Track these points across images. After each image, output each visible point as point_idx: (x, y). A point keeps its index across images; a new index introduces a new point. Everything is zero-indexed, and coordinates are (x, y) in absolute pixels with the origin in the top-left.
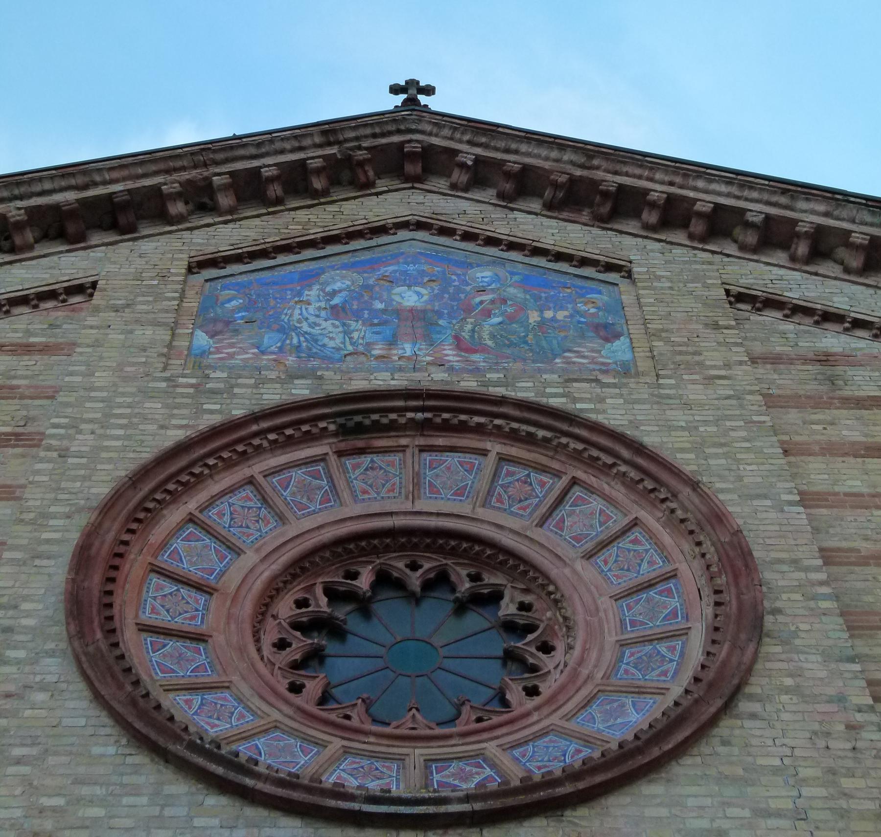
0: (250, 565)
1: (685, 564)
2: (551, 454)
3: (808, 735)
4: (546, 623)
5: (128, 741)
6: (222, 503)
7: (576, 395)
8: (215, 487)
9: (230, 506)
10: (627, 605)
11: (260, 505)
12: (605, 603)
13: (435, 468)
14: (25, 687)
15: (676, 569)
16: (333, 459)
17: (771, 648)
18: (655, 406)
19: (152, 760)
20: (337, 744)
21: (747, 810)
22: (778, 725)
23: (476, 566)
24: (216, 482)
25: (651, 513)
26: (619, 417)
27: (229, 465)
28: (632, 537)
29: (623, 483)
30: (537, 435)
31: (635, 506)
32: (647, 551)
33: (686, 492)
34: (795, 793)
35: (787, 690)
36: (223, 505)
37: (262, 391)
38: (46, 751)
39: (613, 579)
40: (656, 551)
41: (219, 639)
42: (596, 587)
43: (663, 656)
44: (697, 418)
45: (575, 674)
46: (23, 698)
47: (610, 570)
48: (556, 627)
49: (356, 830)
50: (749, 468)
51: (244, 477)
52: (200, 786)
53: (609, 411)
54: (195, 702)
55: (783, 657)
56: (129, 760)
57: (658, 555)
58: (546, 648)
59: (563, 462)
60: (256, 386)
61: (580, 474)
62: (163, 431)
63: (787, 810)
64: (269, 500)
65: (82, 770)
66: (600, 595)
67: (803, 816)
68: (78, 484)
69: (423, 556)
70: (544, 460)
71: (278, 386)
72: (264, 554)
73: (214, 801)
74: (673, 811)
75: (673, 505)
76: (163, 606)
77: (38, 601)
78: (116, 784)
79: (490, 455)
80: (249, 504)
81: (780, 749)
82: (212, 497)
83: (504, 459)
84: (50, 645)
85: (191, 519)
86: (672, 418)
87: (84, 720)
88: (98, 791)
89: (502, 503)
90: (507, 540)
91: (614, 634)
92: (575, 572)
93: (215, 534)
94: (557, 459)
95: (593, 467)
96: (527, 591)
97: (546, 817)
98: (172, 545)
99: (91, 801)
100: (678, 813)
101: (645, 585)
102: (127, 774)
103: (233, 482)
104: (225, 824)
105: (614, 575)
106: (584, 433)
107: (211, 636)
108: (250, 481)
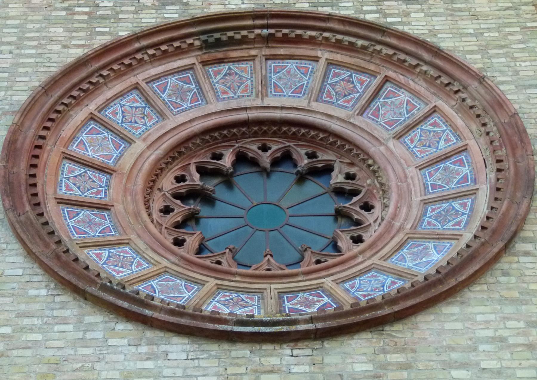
0: (139, 151)
1: (473, 140)
2: (368, 58)
6: (115, 105)
7: (387, 11)
8: (109, 93)
9: (121, 107)
10: (429, 173)
11: (144, 105)
12: (412, 171)
15: (467, 145)
19: (75, 299)
20: (212, 282)
24: (110, 89)
25: (446, 102)
26: (421, 28)
27: (119, 75)
30: (357, 44)
31: (434, 97)
32: (444, 131)
33: (474, 84)
36: (116, 106)
39: (418, 154)
40: (451, 131)
41: (119, 207)
42: (405, 160)
43: (457, 211)
44: (482, 26)
45: (390, 225)
47: (415, 147)
48: (375, 191)
49: (230, 344)
50: (523, 64)
51: (130, 84)
52: (111, 316)
53: (413, 23)
54: (103, 255)
57: (453, 134)
58: (367, 207)
61: (391, 74)
62: (66, 50)
65: (23, 307)
66: (408, 166)
72: (149, 143)
73: (122, 326)
74: (466, 325)
75: (464, 95)
76: (75, 185)
79: (320, 61)
82: (107, 100)
83: (331, 64)
85: (92, 118)
88: (37, 322)
89: (331, 98)
92: (388, 149)
93: (111, 128)
95: (401, 67)
96: (352, 164)
97: (371, 332)
98: (78, 138)
99: (31, 329)
100: (470, 326)
101: (443, 157)
102: (56, 309)
103: (122, 88)
104: (132, 343)
108: (136, 87)
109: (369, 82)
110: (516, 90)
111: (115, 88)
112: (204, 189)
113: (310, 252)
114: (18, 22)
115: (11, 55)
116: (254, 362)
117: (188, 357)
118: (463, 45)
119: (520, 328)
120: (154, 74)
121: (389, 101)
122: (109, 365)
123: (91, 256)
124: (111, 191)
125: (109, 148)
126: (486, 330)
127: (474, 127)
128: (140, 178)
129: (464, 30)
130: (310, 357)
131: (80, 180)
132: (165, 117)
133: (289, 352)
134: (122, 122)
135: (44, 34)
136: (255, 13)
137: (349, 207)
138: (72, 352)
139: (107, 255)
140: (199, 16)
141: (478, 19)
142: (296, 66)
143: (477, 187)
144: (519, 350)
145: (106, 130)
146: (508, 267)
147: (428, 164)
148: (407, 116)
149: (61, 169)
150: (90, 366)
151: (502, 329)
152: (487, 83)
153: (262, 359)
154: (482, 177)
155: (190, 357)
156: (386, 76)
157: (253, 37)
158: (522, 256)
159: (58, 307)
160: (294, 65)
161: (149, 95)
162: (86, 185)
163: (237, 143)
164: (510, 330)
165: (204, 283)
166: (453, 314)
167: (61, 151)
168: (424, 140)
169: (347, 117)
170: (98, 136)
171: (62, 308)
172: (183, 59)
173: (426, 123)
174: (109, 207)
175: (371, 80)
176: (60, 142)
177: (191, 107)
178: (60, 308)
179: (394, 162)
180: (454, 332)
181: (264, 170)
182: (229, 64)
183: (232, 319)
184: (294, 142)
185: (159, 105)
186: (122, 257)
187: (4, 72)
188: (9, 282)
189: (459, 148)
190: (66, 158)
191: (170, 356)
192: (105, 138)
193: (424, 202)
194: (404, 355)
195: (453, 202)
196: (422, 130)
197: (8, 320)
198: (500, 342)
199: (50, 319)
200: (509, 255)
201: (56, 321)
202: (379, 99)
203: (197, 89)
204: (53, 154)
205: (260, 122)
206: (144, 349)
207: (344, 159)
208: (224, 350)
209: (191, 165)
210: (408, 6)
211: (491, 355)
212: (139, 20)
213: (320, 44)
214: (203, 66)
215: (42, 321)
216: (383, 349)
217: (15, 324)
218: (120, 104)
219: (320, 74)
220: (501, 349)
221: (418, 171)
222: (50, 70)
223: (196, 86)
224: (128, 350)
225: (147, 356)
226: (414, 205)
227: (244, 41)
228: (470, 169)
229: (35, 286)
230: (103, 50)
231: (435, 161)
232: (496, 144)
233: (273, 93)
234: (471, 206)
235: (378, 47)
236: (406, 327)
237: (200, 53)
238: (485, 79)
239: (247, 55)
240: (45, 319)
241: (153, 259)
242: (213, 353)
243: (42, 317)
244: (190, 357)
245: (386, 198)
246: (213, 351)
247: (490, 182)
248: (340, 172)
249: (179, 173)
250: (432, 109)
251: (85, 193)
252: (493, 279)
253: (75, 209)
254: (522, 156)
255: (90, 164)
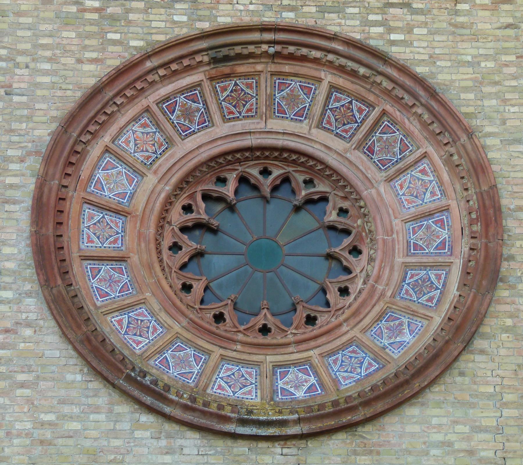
0: (151, 187)
1: (455, 202)
2: (368, 87)
3: (514, 367)
4: (357, 230)
5: (88, 370)
6: (128, 131)
7: (391, 23)
8: (122, 120)
9: (134, 134)
10: (413, 228)
11: (155, 130)
12: (397, 224)
13: (283, 91)
14: (17, 323)
15: (449, 205)
16: (206, 84)
17: (503, 293)
18: (451, 38)
19: (105, 386)
20: (218, 352)
21: (468, 427)
22: (497, 360)
23: (310, 174)
24: (123, 115)
25: (436, 151)
26: (421, 50)
27: (131, 99)
28: (421, 168)
29: (420, 121)
30: (359, 72)
31: (426, 142)
32: (431, 182)
33: (464, 138)
34: (499, 414)
35: (506, 330)
36: (129, 134)
37: (151, 17)
38: (38, 377)
39: (405, 203)
40: (437, 183)
41: (135, 258)
42: (393, 210)
43: (432, 283)
44: (481, 51)
45: (373, 289)
46: (17, 333)
47: (404, 194)
48: (364, 234)
49: (232, 441)
50: (512, 110)
51: (142, 108)
52: (136, 407)
53: (415, 44)
54: (124, 321)
55: (509, 300)
56: (91, 385)
57: (439, 187)
58: (355, 251)
59: (378, 96)
60: (145, 11)
61: (389, 108)
62: (79, 66)
63: (492, 427)
64: (161, 125)
65: (63, 393)
66: (396, 218)
67: (501, 432)
68: (24, 125)
69: (272, 164)
70: (363, 92)
71: (162, 11)
72: (160, 175)
73: (146, 418)
74: (423, 428)
75: (453, 150)
76: (95, 234)
77: (13, 246)
78: (85, 405)
79: (323, 82)
80: (148, 130)
81: (495, 379)
82: (121, 129)
83: (334, 87)
84: (28, 287)
85: (107, 150)
86: (462, 51)
87: (58, 352)
88: (76, 410)
89: (331, 125)
90: (332, 160)
91: (401, 255)
92: (379, 194)
93: (125, 161)
94: (372, 92)
95: (399, 103)
96: (345, 198)
97: (346, 432)
98: (95, 176)
99: (71, 417)
100: (426, 430)
101: (427, 214)
102: (90, 397)
103: (135, 113)
104: (154, 435)
105: (406, 200)
106: (394, 73)
107: (129, 257)
109: (368, 112)
110: (501, 146)
111: (128, 114)
112: (210, 224)
113: (301, 307)
114: (30, 20)
115: (27, 70)
116: (252, 460)
117: (199, 452)
118: (460, 78)
119: (466, 433)
120: (164, 94)
121: (385, 136)
122: (136, 458)
123: (114, 325)
124: (127, 238)
125: (123, 184)
126: (438, 434)
127: (458, 187)
128: (152, 221)
129: (463, 57)
130: (296, 457)
131: (99, 227)
132: (174, 144)
133: (278, 450)
134: (135, 152)
135: (58, 40)
136: (263, 26)
137: (339, 252)
138: (105, 443)
139: (127, 321)
140: (208, 30)
141: (478, 41)
142: (300, 85)
143: (452, 261)
144: (461, 455)
145: (120, 163)
146: (465, 366)
147: (413, 219)
148: (399, 157)
149: (82, 216)
150: (121, 458)
151: (450, 433)
152: (474, 141)
153: (258, 457)
154: (457, 250)
155: (200, 453)
156: (384, 110)
157: (259, 53)
158: (477, 354)
159: (91, 394)
160: (298, 84)
161: (159, 119)
162: (105, 233)
163: (241, 166)
164: (457, 435)
165: (211, 353)
166: (413, 417)
167: (81, 197)
168: (413, 188)
169: (344, 150)
170: (112, 171)
171: (95, 396)
172: (192, 75)
173: (416, 169)
174: (126, 259)
175: (369, 110)
176: (80, 186)
177: (198, 129)
178: (93, 396)
179: (383, 210)
180: (413, 435)
181: (264, 198)
182: (235, 79)
183: (235, 417)
184: (293, 167)
185: (168, 130)
186: (139, 322)
187: (23, 95)
188: (49, 365)
189: (442, 207)
190: (86, 203)
191: (186, 451)
192: (119, 173)
193: (405, 264)
194: (370, 457)
195: (430, 270)
196: (412, 176)
197: (52, 407)
198: (447, 447)
199: (86, 407)
200: (467, 353)
201: (91, 409)
202: (376, 133)
203: (205, 109)
204: (74, 201)
205: (262, 148)
206: (163, 443)
207: (338, 191)
208: (228, 446)
209: (198, 193)
210: (413, 17)
211: (439, 460)
212: (148, 24)
213: (324, 65)
214: (211, 81)
215: (80, 409)
216: (355, 450)
217: (57, 411)
218: (133, 130)
219: (322, 98)
220: (448, 454)
221: (404, 224)
222: (66, 94)
223: (204, 105)
224: (151, 443)
225: (166, 451)
226: (396, 268)
227: (316, 61)
228: (449, 233)
229: (71, 371)
230: (116, 74)
231: (419, 216)
232: (474, 216)
233: (277, 114)
234: (444, 281)
235: (379, 79)
236: (375, 428)
237: (207, 68)
238: (473, 136)
239: (253, 70)
240: (82, 407)
241: (166, 323)
242: (219, 449)
243: (79, 405)
244: (200, 453)
245: (373, 249)
246: (219, 447)
247: (464, 258)
248: (334, 208)
249: (186, 202)
250: (422, 154)
251: (104, 243)
252: (450, 379)
253: (96, 265)
254: (494, 235)
255: (108, 208)
